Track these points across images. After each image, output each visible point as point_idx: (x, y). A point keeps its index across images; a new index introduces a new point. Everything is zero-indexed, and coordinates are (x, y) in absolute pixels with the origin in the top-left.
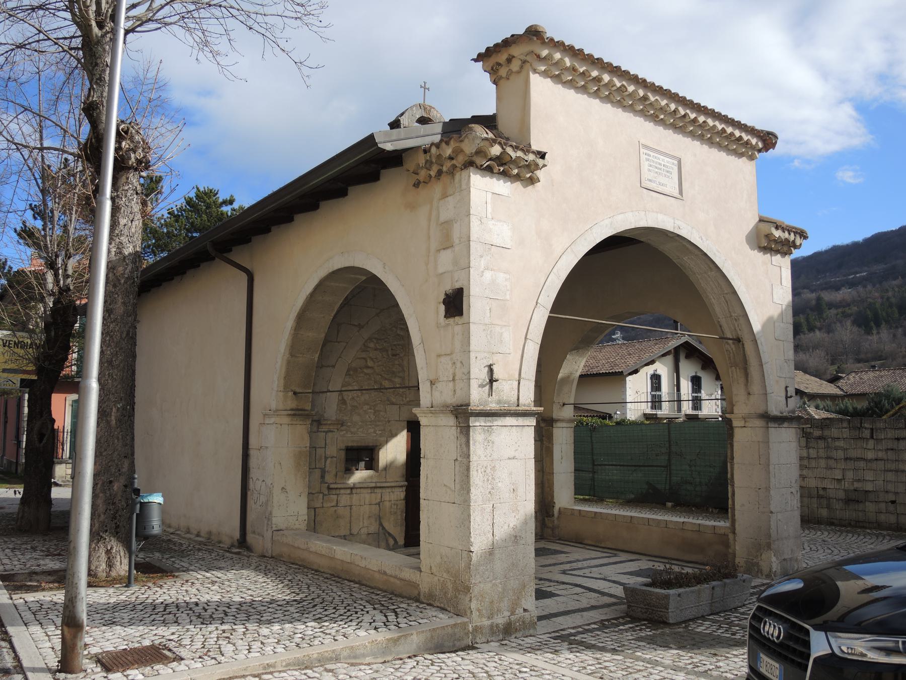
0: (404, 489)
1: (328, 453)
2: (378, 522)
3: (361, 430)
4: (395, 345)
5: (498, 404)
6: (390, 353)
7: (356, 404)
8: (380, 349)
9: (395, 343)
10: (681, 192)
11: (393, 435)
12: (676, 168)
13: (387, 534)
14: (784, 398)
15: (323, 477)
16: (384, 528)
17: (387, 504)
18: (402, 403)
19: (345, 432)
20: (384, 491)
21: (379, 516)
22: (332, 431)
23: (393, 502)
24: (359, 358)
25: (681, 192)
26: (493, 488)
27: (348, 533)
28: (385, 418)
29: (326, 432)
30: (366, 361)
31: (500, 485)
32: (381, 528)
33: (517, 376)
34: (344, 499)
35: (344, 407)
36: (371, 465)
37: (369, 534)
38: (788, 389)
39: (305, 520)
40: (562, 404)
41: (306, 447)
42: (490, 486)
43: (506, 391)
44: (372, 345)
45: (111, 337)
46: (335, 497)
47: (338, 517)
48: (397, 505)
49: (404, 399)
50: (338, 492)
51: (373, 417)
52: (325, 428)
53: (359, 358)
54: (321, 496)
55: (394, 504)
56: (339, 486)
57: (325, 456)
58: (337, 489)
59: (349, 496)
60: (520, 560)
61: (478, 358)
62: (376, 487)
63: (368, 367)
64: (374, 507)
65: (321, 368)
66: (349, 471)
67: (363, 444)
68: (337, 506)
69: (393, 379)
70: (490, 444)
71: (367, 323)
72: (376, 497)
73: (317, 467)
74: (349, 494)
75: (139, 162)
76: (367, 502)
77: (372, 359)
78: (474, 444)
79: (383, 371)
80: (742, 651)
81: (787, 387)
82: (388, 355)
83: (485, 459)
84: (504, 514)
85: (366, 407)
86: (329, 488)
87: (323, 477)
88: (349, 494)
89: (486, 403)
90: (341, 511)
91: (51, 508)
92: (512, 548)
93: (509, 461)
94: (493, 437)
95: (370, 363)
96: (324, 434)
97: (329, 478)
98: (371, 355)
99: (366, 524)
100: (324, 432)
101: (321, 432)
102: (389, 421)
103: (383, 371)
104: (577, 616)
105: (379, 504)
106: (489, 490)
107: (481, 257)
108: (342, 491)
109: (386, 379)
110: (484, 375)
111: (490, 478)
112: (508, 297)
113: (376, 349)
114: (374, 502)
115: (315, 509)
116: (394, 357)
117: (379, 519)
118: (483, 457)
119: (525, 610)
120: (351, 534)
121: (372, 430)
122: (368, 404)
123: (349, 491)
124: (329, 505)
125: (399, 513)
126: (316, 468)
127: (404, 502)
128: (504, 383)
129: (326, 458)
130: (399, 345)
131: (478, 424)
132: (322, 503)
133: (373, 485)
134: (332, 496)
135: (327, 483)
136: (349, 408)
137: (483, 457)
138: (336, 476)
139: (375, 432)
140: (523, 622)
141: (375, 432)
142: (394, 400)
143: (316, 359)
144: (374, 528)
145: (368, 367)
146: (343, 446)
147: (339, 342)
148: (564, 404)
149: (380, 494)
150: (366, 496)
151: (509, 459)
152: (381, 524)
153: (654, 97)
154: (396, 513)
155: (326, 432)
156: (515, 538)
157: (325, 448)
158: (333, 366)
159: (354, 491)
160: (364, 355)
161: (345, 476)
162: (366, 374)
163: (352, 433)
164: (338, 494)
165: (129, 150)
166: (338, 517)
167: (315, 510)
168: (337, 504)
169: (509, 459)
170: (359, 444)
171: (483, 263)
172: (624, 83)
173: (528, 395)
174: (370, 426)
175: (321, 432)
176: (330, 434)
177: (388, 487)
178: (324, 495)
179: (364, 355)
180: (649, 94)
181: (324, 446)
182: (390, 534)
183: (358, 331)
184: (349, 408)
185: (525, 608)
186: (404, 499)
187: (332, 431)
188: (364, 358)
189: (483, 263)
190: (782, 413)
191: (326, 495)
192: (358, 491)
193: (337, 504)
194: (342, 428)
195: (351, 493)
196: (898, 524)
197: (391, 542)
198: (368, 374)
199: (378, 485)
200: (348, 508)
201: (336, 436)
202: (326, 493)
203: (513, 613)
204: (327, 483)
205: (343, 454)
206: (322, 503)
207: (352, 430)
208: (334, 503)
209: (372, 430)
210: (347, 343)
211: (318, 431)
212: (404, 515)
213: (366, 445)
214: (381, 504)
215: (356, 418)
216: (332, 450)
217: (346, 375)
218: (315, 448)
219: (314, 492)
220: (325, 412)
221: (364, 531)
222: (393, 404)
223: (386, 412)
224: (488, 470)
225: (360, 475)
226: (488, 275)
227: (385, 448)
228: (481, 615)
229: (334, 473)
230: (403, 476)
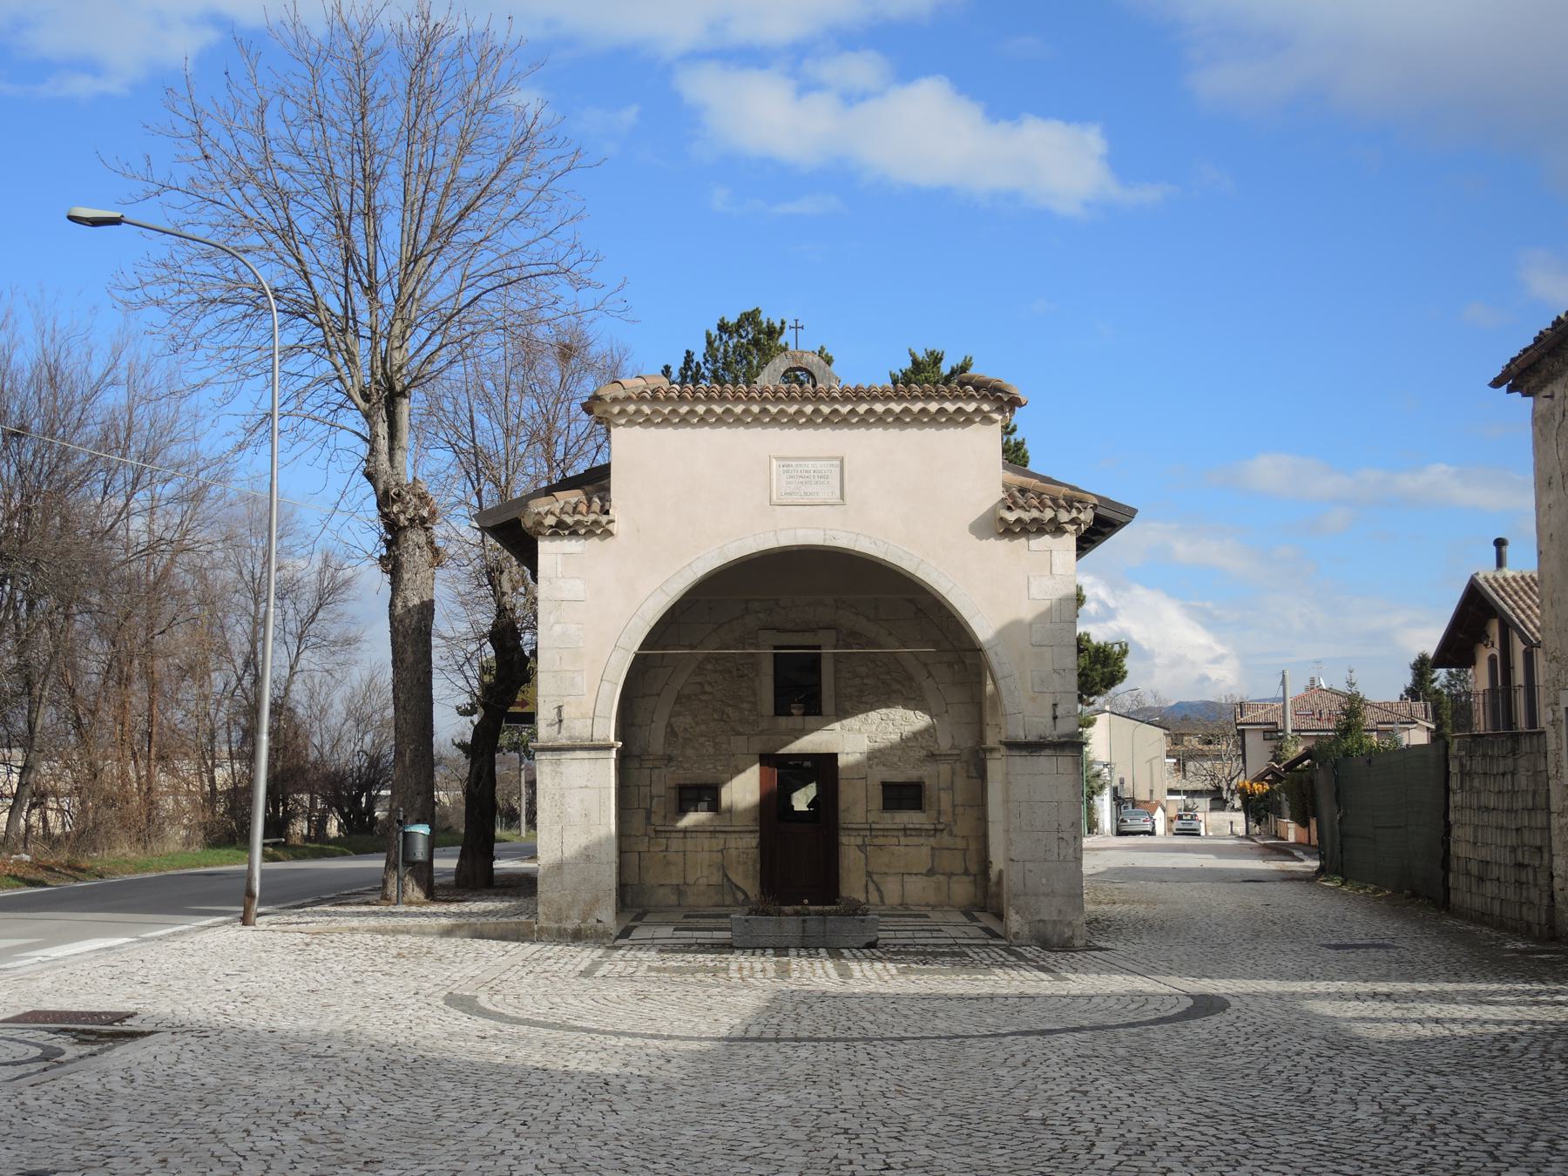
0: (758, 835)
1: (654, 792)
3: (696, 765)
6: (735, 673)
9: (742, 662)
10: (842, 497)
11: (739, 771)
12: (838, 469)
14: (1051, 719)
15: (648, 818)
16: (729, 880)
17: (733, 852)
25: (842, 497)
29: (652, 769)
30: (703, 686)
31: (569, 810)
33: (591, 715)
34: (676, 844)
36: (714, 806)
37: (709, 885)
43: (578, 728)
44: (709, 667)
45: (404, 684)
46: (664, 841)
47: (668, 863)
48: (747, 854)
50: (668, 835)
51: (711, 750)
52: (649, 764)
54: (646, 839)
56: (669, 828)
58: (665, 831)
62: (716, 832)
63: (705, 693)
64: (715, 855)
66: (682, 811)
67: (699, 782)
68: (666, 851)
70: (559, 775)
71: (702, 642)
72: (717, 843)
75: (412, 520)
76: (706, 848)
77: (710, 683)
78: (541, 775)
80: (442, 881)
81: (1055, 705)
87: (648, 818)
89: (555, 739)
90: (671, 856)
91: (462, 851)
94: (563, 769)
95: (708, 688)
97: (656, 819)
98: (708, 678)
99: (705, 874)
102: (733, 755)
105: (722, 851)
107: (550, 613)
108: (674, 835)
109: (729, 705)
110: (553, 714)
112: (581, 644)
114: (715, 849)
117: (723, 869)
118: (550, 786)
119: (598, 921)
120: (685, 883)
121: (711, 766)
122: (705, 736)
123: (681, 835)
128: (576, 721)
129: (652, 798)
131: (544, 757)
133: (712, 829)
136: (681, 740)
137: (550, 786)
138: (665, 817)
139: (715, 768)
140: (596, 931)
141: (715, 768)
142: (741, 730)
144: (716, 878)
145: (705, 693)
150: (705, 842)
152: (725, 875)
153: (775, 407)
154: (745, 863)
155: (652, 769)
156: (587, 855)
158: (659, 695)
159: (688, 835)
160: (699, 679)
162: (701, 701)
165: (399, 512)
166: (668, 863)
170: (694, 782)
171: (552, 618)
172: (728, 406)
173: (607, 730)
176: (656, 771)
177: (734, 832)
178: (650, 838)
179: (699, 679)
180: (768, 407)
181: (648, 783)
182: (738, 887)
184: (681, 740)
188: (700, 683)
189: (552, 618)
192: (694, 834)
195: (685, 837)
196: (1501, 916)
197: (740, 897)
199: (718, 829)
202: (653, 835)
203: (584, 921)
205: (673, 794)
207: (686, 766)
208: (664, 848)
209: (711, 766)
211: (641, 768)
213: (704, 782)
215: (689, 752)
216: (659, 789)
217: (675, 703)
221: (703, 881)
223: (729, 744)
224: (557, 797)
225: (691, 819)
226: (558, 628)
227: (729, 785)
228: (548, 918)
229: (662, 813)
230: (756, 819)
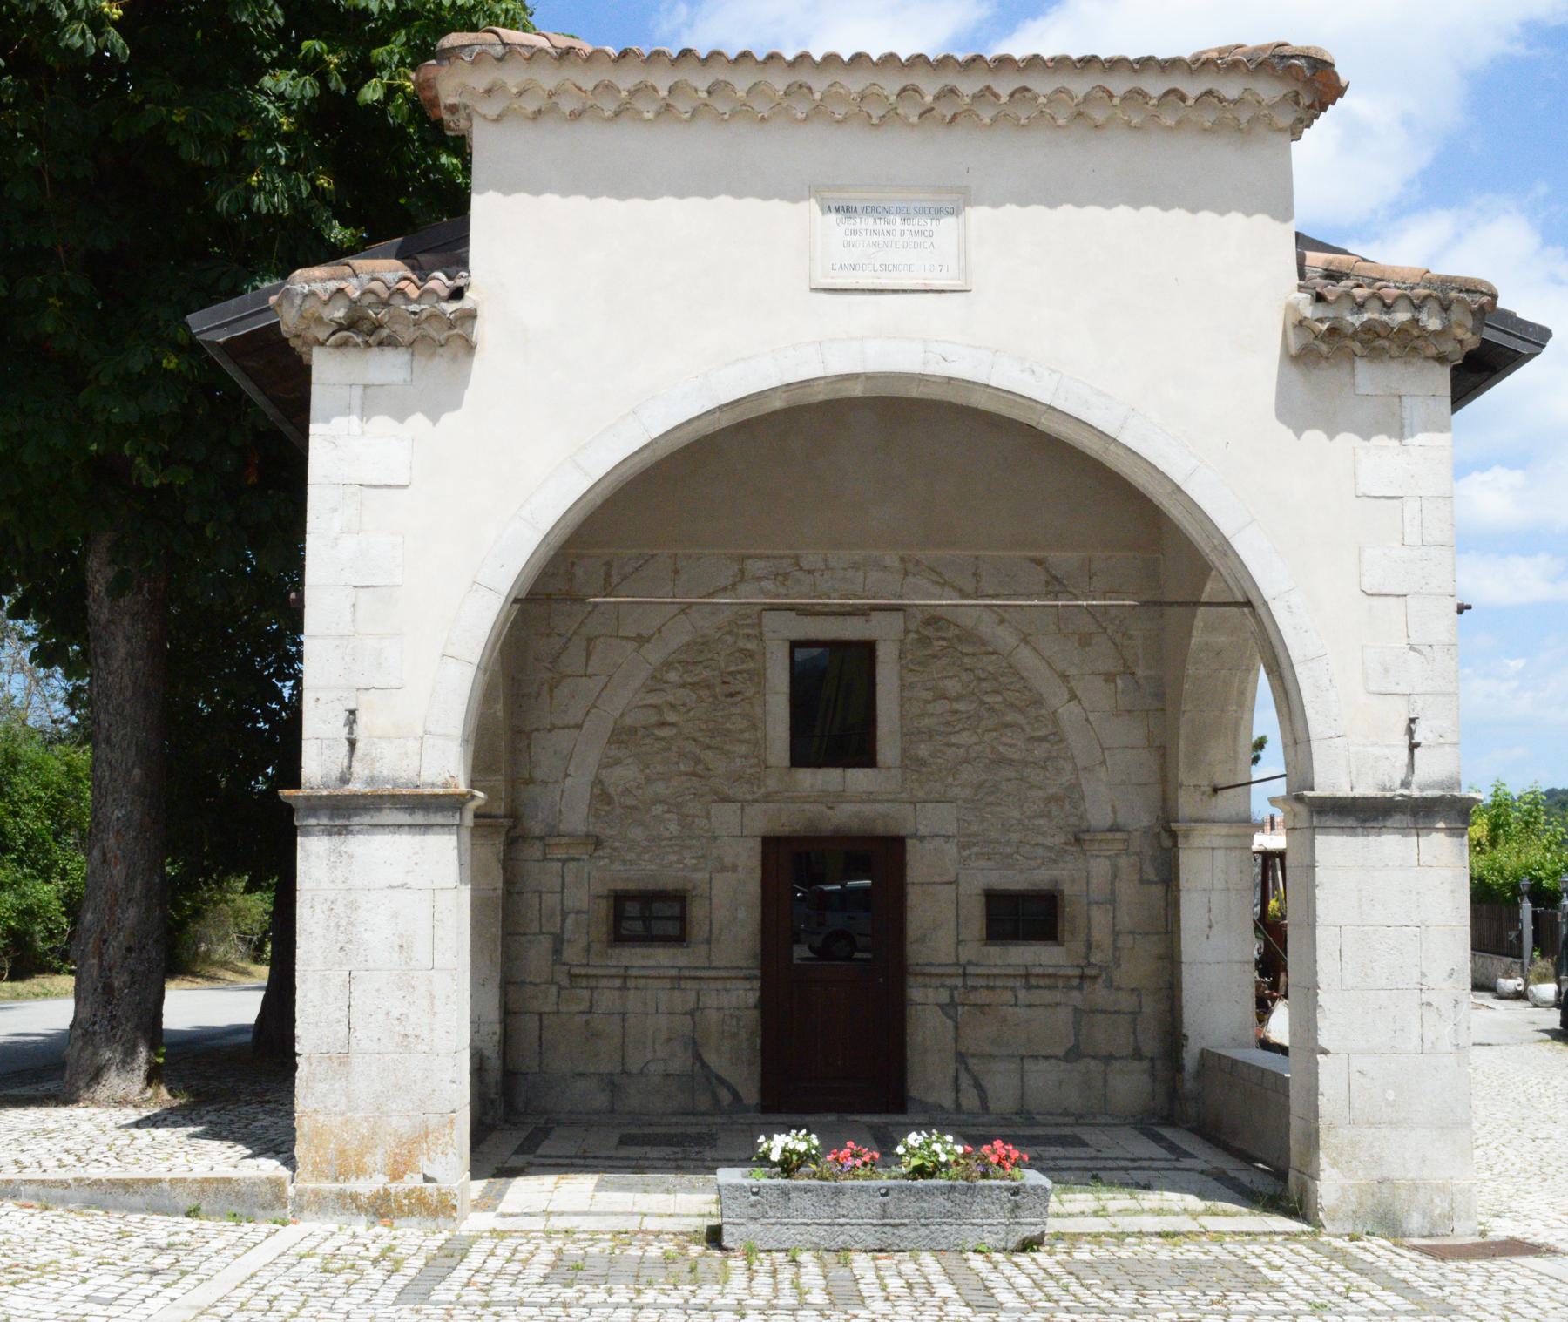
1: (569, 903)
2: (689, 1054)
4: (731, 673)
5: (368, 784)
7: (635, 803)
8: (693, 684)
13: (715, 1082)
14: (1406, 751)
16: (704, 1065)
17: (713, 1016)
18: (749, 797)
19: (606, 861)
20: (704, 985)
21: (693, 1038)
22: (578, 860)
23: (727, 1012)
24: (638, 707)
26: (349, 942)
27: (619, 1070)
28: (707, 831)
31: (366, 936)
32: (698, 1064)
35: (607, 808)
37: (668, 1075)
38: (1416, 727)
39: (494, 1033)
40: (1208, 790)
41: (495, 889)
42: (342, 938)
44: (673, 676)
46: (586, 994)
49: (755, 789)
50: (593, 983)
53: (638, 707)
54: (554, 989)
55: (732, 1016)
57: (562, 910)
59: (617, 993)
60: (415, 1082)
61: (322, 700)
63: (663, 724)
65: (550, 730)
68: (590, 1012)
69: (727, 747)
70: (345, 859)
72: (685, 998)
73: (544, 930)
74: (619, 989)
77: (673, 706)
79: (701, 730)
81: (1412, 721)
82: (715, 697)
83: (332, 886)
84: (378, 990)
85: (658, 809)
86: (572, 977)
88: (619, 989)
92: (396, 1056)
93: (390, 891)
95: (671, 717)
96: (560, 864)
97: (571, 954)
100: (559, 860)
101: (553, 860)
102: (716, 838)
103: (701, 730)
104: (623, 1218)
105: (691, 1013)
106: (340, 945)
107: (335, 510)
108: (604, 983)
109: (709, 747)
111: (343, 923)
113: (683, 686)
115: (540, 1014)
116: (729, 700)
117: (695, 1047)
119: (427, 1179)
120: (624, 1072)
122: (662, 802)
124: (575, 1008)
125: (743, 1034)
126: (541, 933)
127: (756, 1014)
130: (740, 672)
132: (558, 1004)
134: (578, 991)
135: (565, 964)
139: (680, 861)
141: (680, 861)
143: (500, 714)
144: (680, 1062)
146: (602, 889)
147: (590, 677)
148: (1216, 790)
149: (694, 994)
151: (391, 887)
152: (698, 1057)
154: (735, 1035)
155: (564, 861)
157: (562, 892)
161: (609, 951)
162: (658, 739)
163: (624, 862)
164: (592, 989)
167: (541, 1020)
168: (591, 1007)
169: (391, 887)
170: (642, 887)
174: (668, 849)
175: (553, 860)
176: (572, 865)
178: (560, 988)
179: (653, 699)
183: (637, 650)
184: (618, 811)
185: (430, 1174)
186: (756, 1007)
187: (578, 860)
190: (1384, 789)
191: (565, 988)
193: (591, 1007)
194: (600, 853)
195: (624, 988)
198: (663, 739)
199: (686, 973)
200: (617, 1018)
201: (586, 870)
204: (565, 964)
206: (558, 1004)
208: (584, 1006)
209: (673, 858)
210: (610, 676)
211: (545, 859)
212: (759, 1041)
214: (698, 1014)
218: (540, 892)
219: (538, 981)
220: (560, 821)
222: (726, 799)
223: (708, 816)
224: (339, 908)
229: (583, 942)
